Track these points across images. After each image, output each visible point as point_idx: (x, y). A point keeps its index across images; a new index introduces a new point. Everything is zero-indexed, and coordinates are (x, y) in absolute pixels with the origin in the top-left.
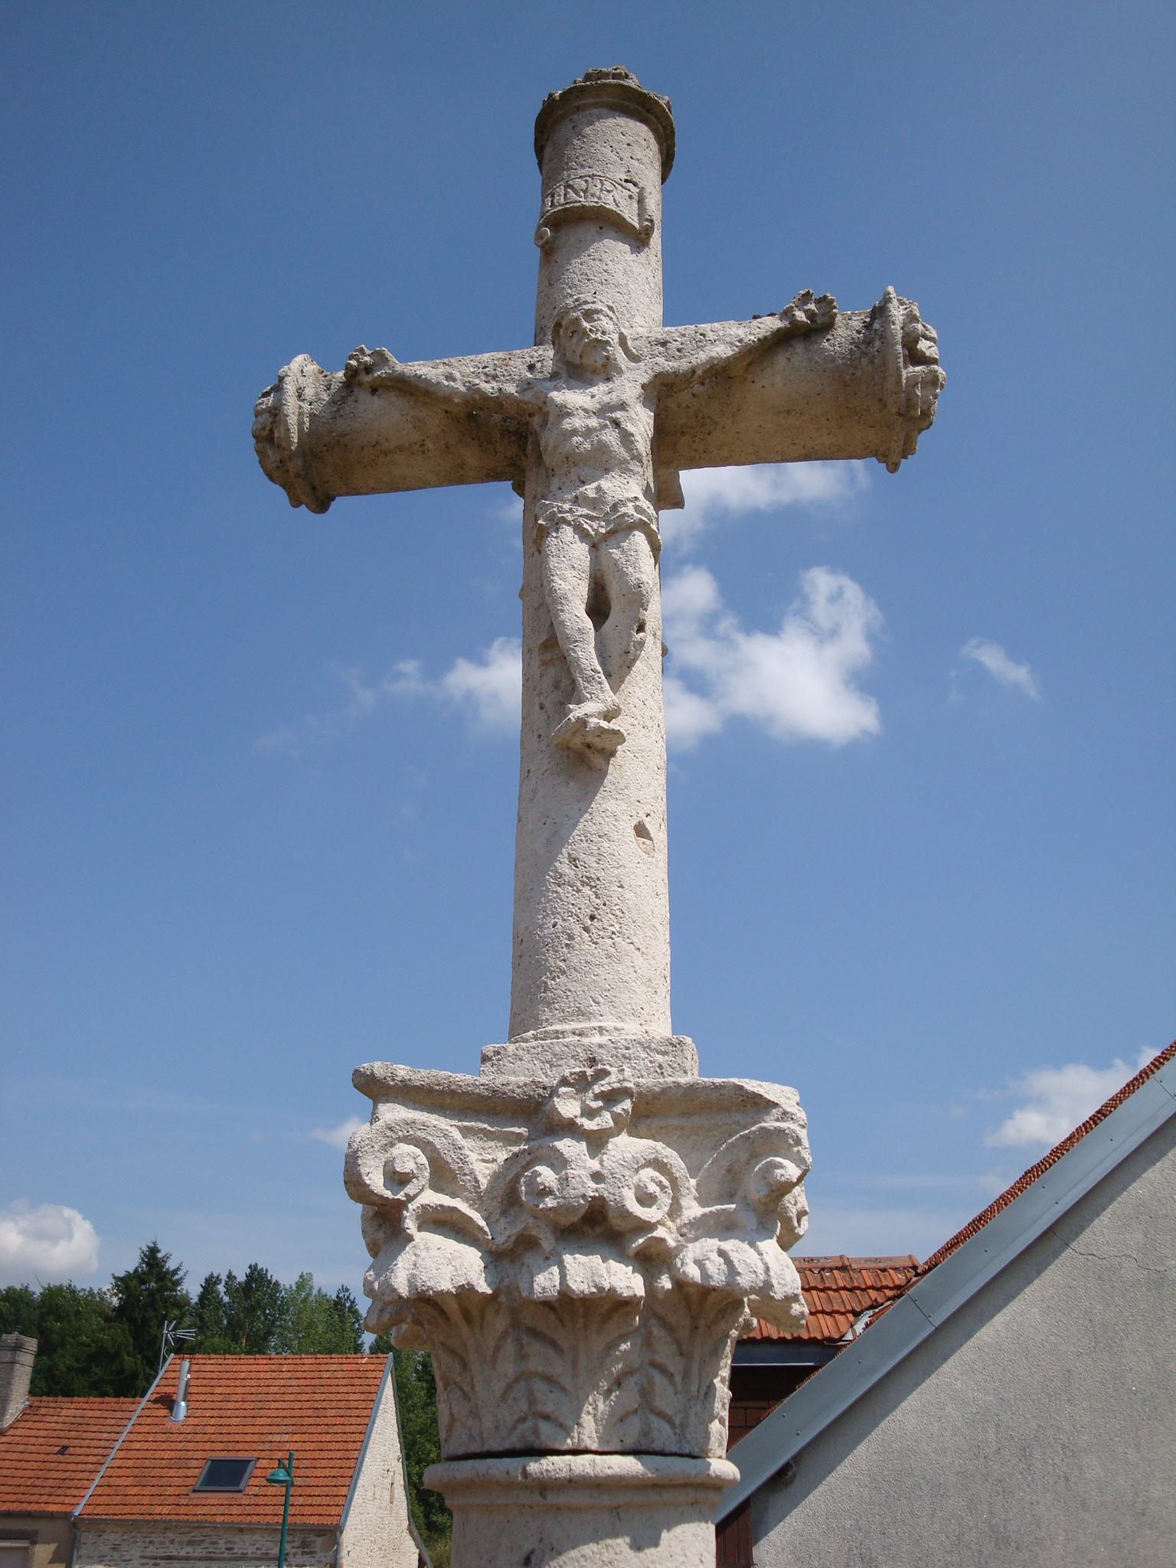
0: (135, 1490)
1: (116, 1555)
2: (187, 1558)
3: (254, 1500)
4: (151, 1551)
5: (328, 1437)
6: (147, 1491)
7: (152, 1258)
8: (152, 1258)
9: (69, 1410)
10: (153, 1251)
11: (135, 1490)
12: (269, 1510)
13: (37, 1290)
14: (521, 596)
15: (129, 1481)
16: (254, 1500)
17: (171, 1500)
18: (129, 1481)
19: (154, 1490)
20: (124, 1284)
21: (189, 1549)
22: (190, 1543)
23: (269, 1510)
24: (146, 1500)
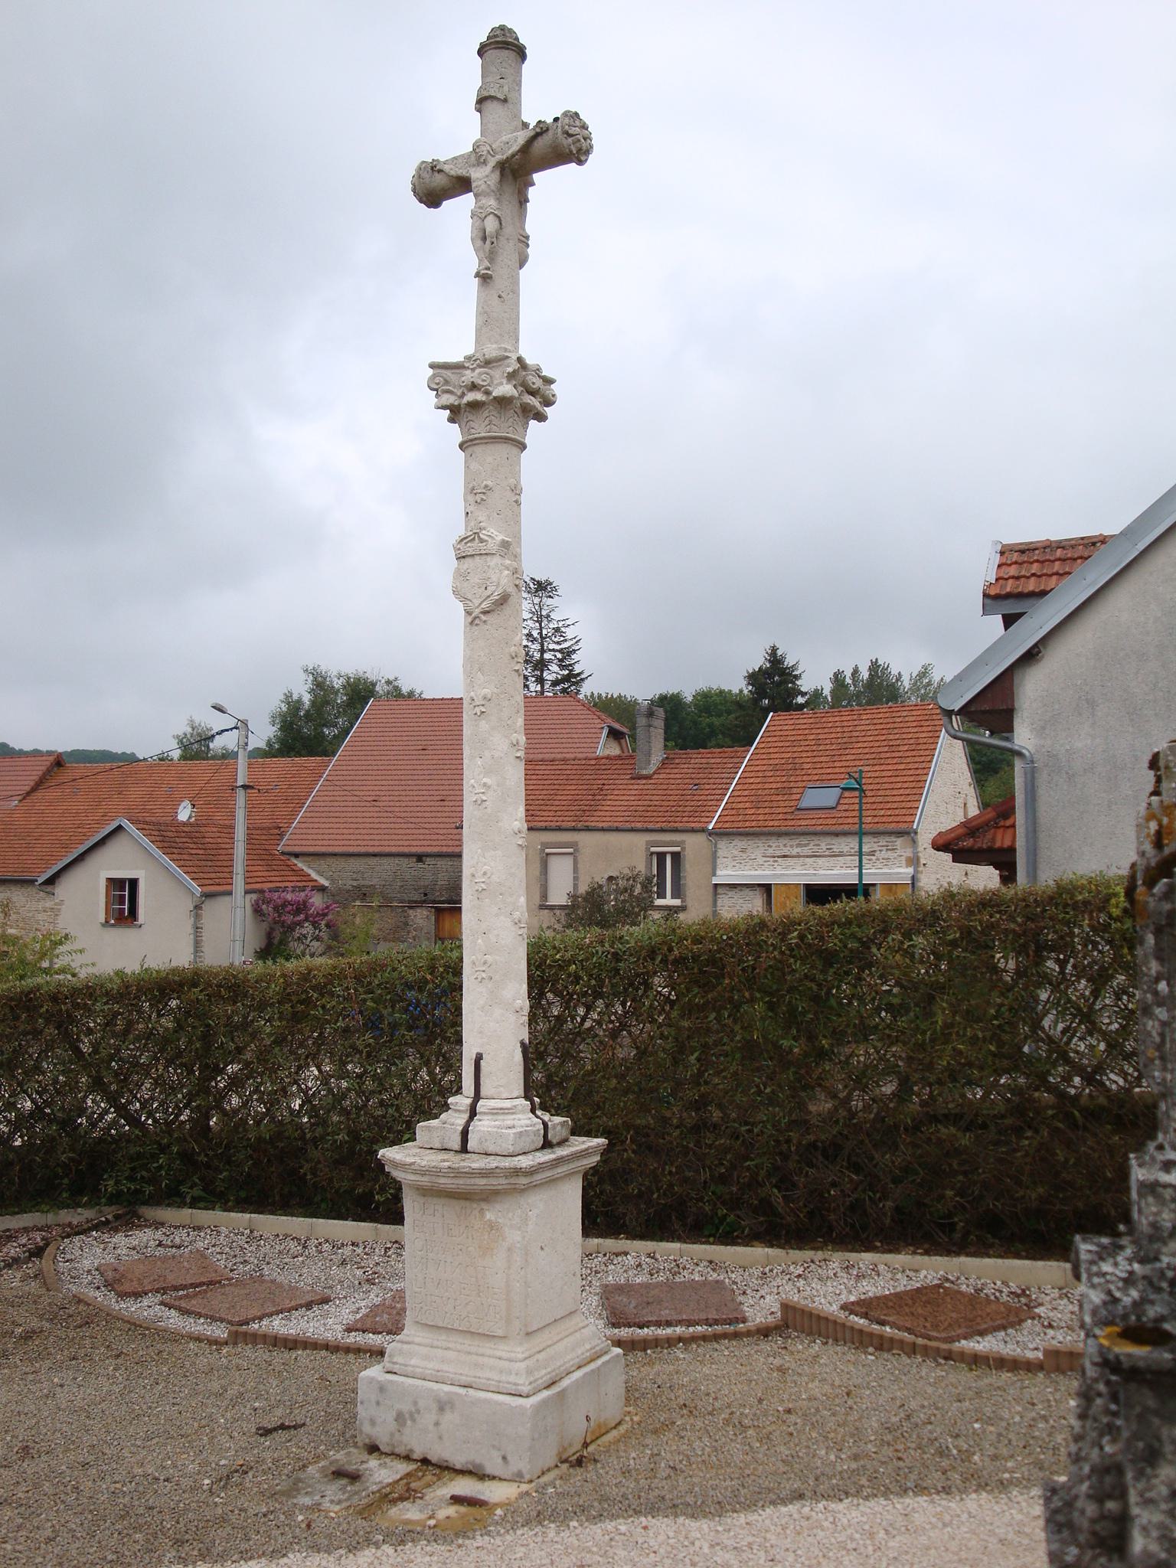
0: (752, 811)
1: (744, 856)
2: (799, 856)
3: (844, 814)
4: (770, 851)
5: (902, 767)
6: (761, 811)
7: (775, 659)
8: (775, 659)
9: (697, 758)
10: (774, 650)
11: (752, 811)
12: (850, 820)
13: (688, 697)
14: (591, 147)
15: (747, 805)
16: (844, 814)
17: (781, 816)
18: (747, 805)
19: (767, 811)
20: (753, 678)
21: (799, 850)
22: (799, 845)
23: (850, 820)
24: (761, 817)
